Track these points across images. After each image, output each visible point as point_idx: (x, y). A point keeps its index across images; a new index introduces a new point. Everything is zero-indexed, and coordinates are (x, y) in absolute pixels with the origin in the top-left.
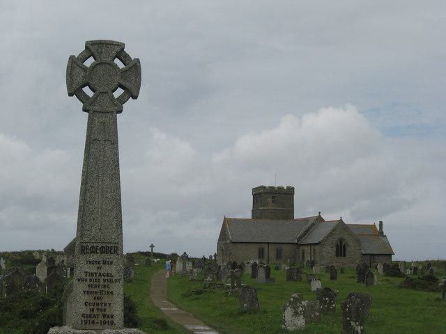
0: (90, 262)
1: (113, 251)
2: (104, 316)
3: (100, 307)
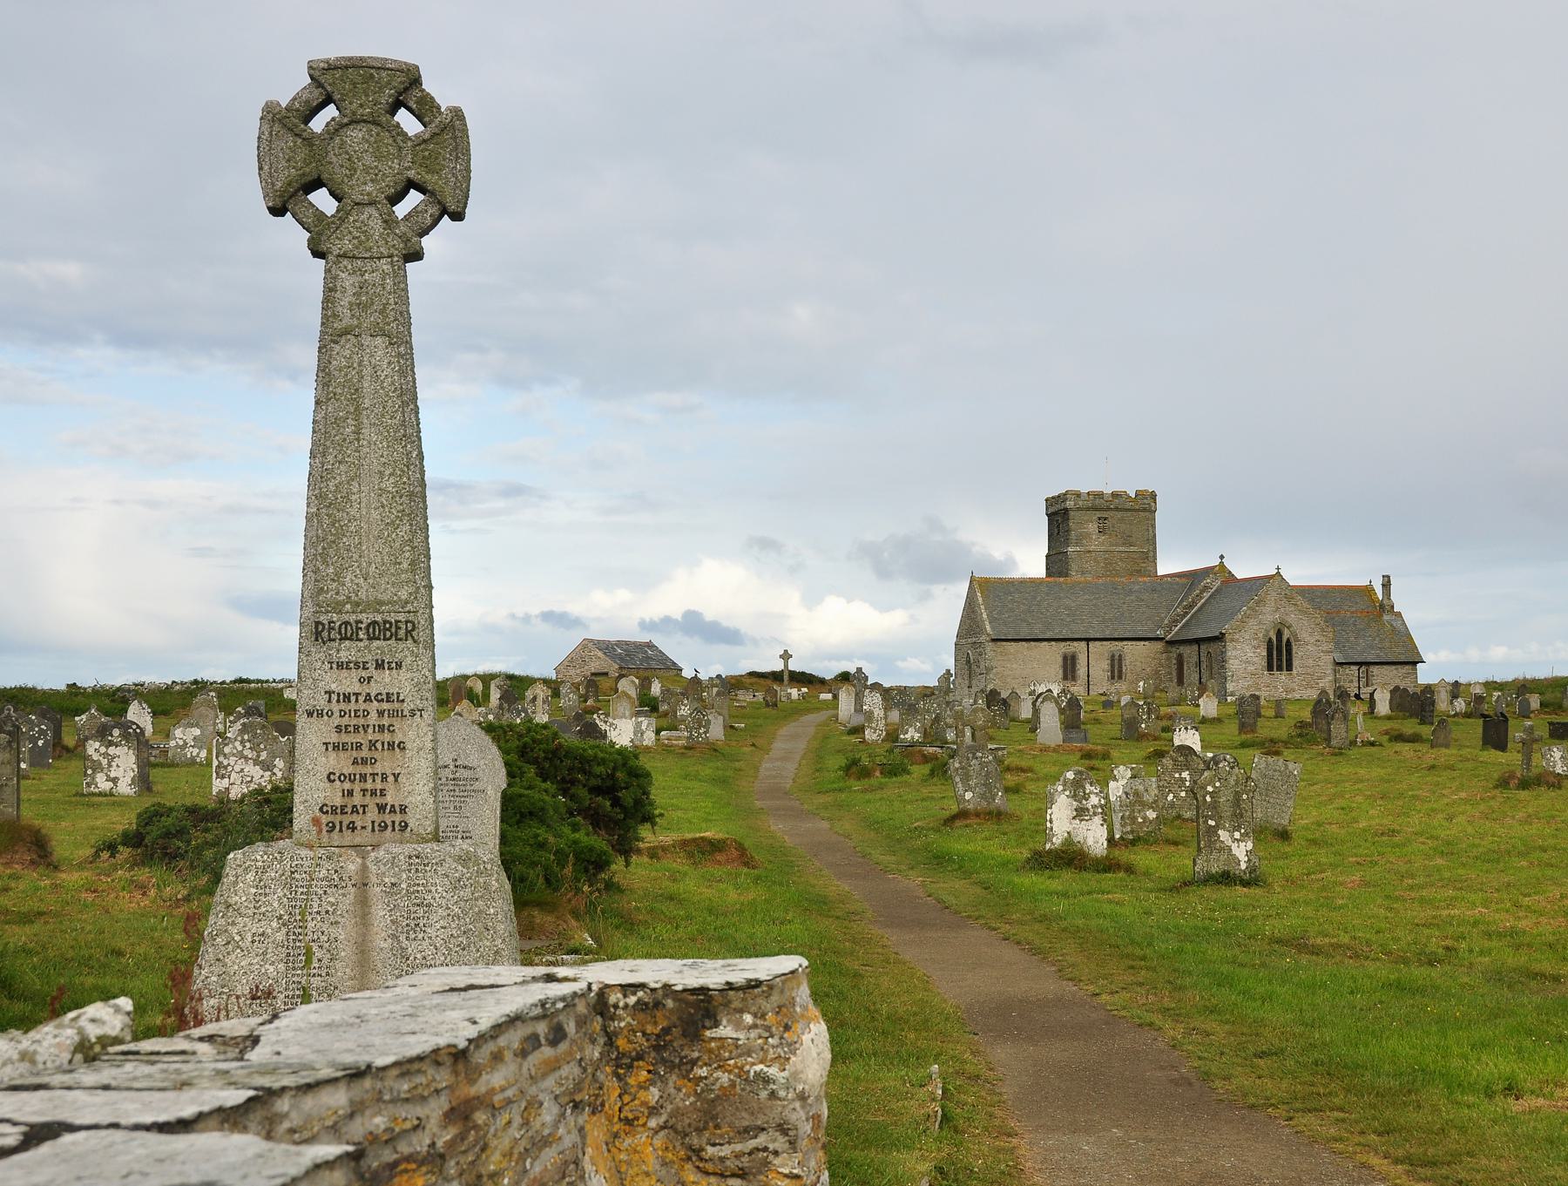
0: (340, 666)
1: (402, 633)
2: (381, 808)
3: (369, 785)
